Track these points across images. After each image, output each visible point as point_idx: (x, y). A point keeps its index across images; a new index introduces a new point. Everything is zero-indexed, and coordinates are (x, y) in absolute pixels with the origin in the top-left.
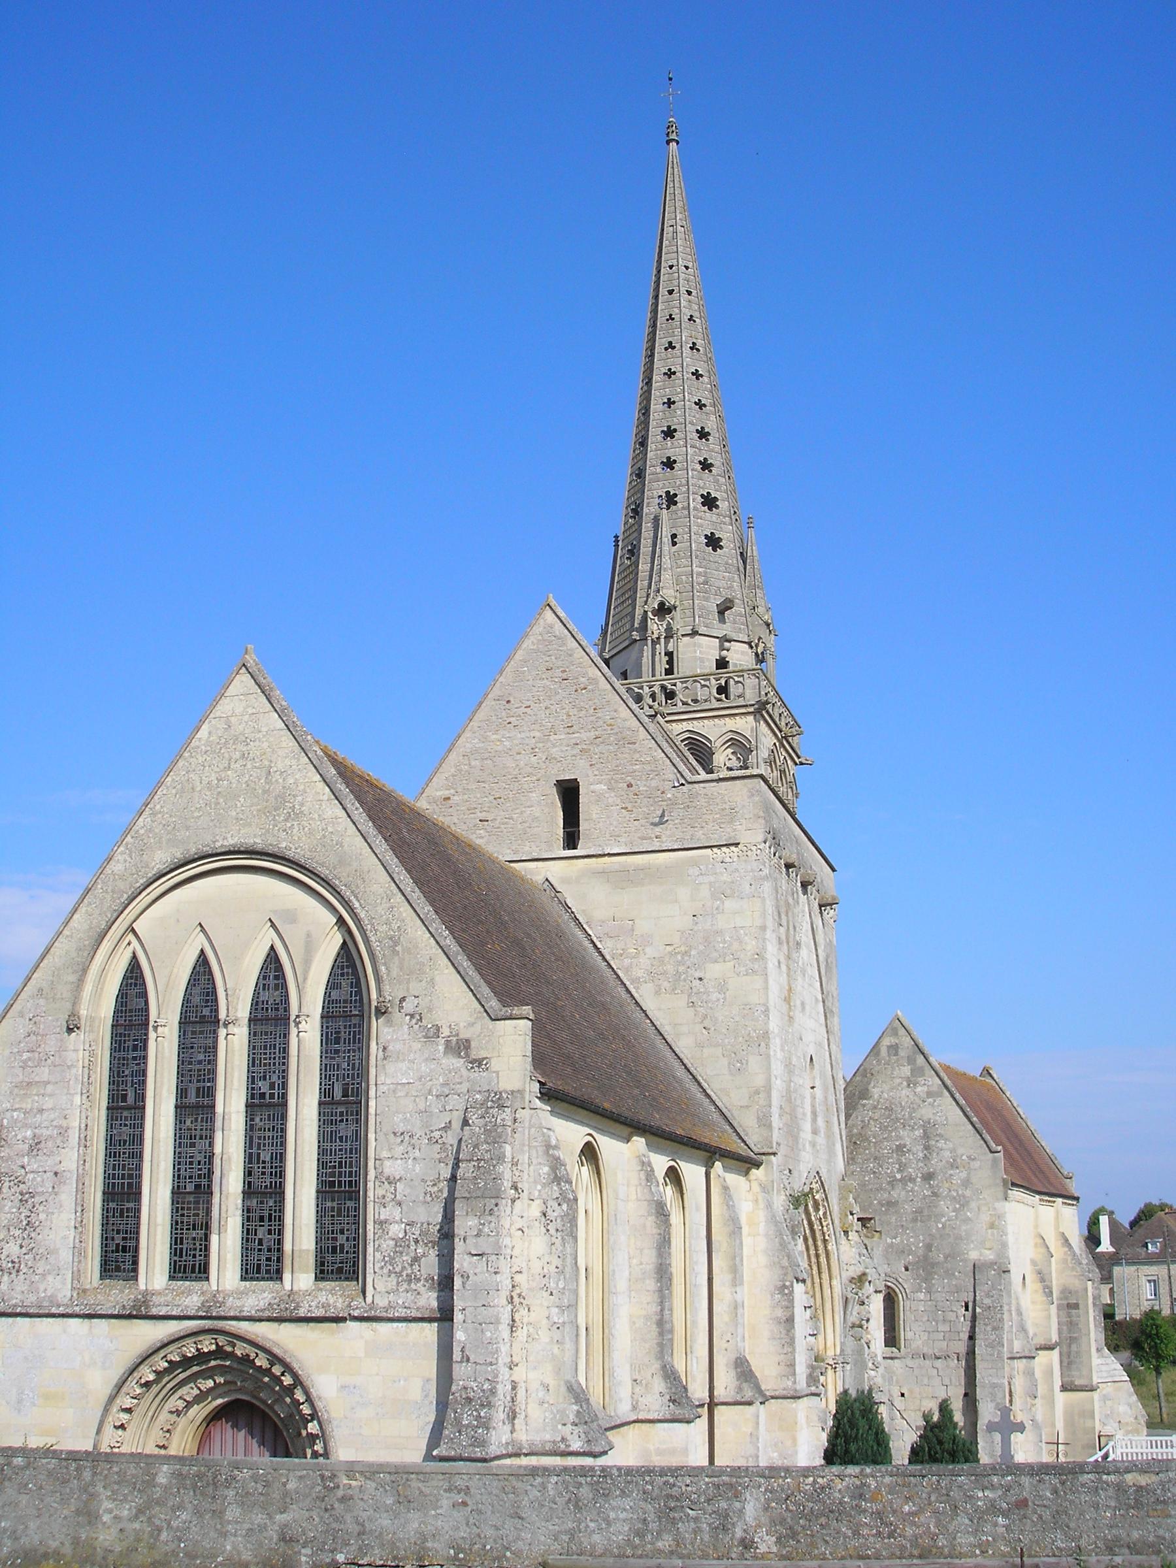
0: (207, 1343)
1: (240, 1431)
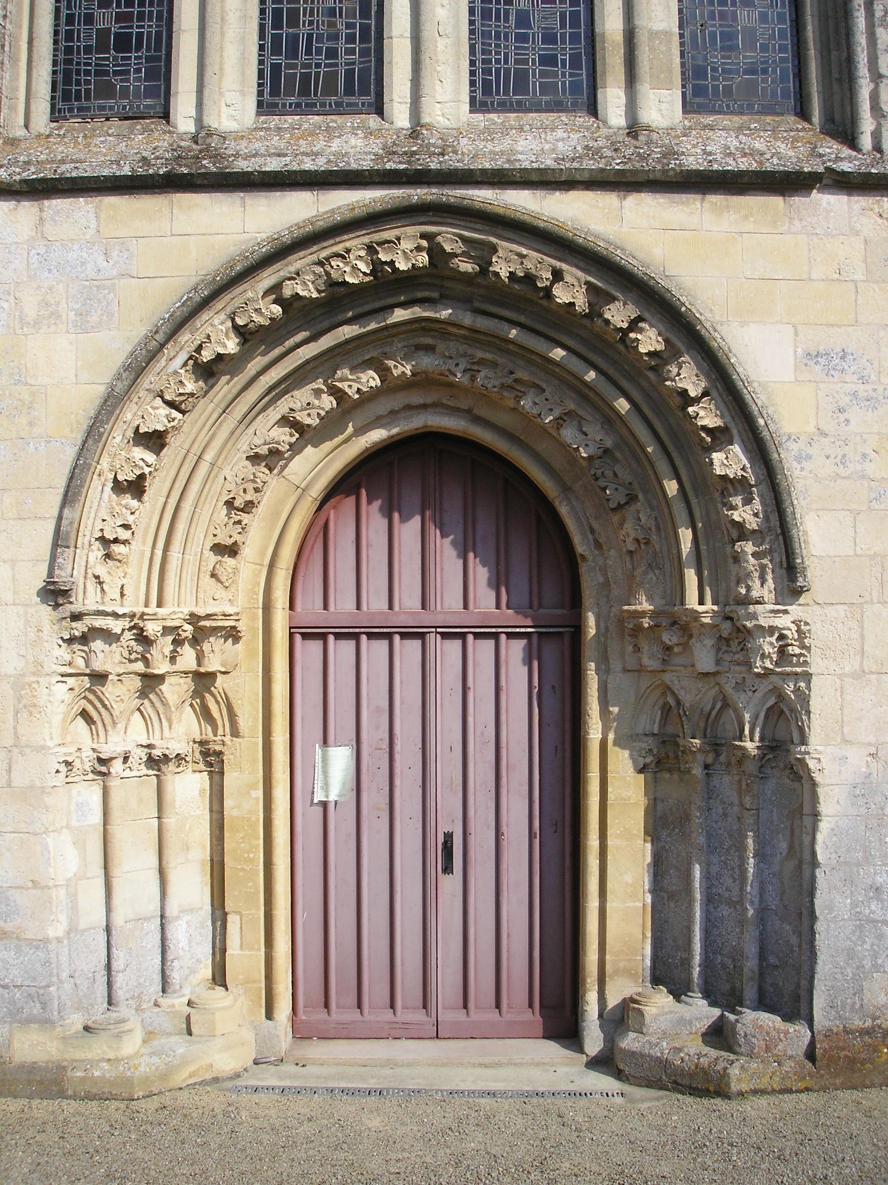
0: (407, 245)
1: (404, 519)
